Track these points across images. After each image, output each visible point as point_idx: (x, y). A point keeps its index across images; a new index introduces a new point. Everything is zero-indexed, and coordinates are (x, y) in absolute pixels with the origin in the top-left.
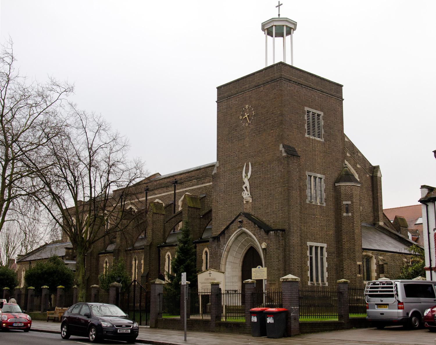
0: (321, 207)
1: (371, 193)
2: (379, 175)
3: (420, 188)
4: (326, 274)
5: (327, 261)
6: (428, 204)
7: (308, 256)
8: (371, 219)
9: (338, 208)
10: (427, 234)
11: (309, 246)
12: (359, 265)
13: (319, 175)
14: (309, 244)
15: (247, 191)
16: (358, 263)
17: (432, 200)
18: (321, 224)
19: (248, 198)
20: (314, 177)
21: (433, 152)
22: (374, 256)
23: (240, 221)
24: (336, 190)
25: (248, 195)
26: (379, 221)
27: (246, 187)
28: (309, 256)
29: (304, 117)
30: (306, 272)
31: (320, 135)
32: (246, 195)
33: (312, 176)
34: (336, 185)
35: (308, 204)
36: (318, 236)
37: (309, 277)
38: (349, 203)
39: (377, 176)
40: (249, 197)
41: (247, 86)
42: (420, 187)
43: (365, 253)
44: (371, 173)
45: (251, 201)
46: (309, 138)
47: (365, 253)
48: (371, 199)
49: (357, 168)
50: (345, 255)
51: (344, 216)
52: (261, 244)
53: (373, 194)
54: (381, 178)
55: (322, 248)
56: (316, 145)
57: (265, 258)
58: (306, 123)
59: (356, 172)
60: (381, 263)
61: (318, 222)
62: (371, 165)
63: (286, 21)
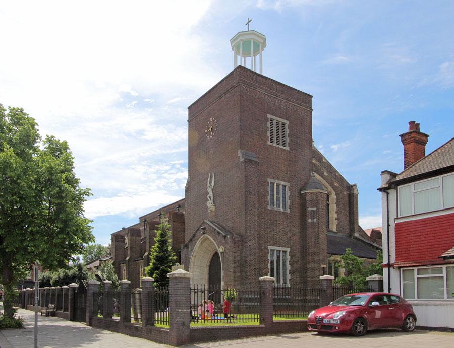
0: (284, 213)
1: (347, 208)
2: (355, 192)
3: (381, 175)
4: (289, 277)
5: (290, 264)
6: (389, 191)
8: (348, 231)
9: (303, 215)
10: (387, 227)
12: (323, 268)
16: (323, 266)
17: (393, 186)
20: (283, 185)
21: (400, 136)
23: (202, 228)
24: (302, 197)
26: (354, 233)
27: (210, 197)
29: (266, 124)
32: (210, 204)
33: (280, 184)
36: (280, 241)
38: (315, 209)
39: (353, 194)
41: (211, 99)
42: (381, 173)
43: (333, 258)
44: (348, 191)
45: (214, 210)
46: (272, 146)
47: (333, 258)
48: (348, 214)
49: (335, 186)
50: (310, 258)
52: (219, 248)
53: (350, 209)
54: (357, 195)
56: (280, 153)
57: (223, 260)
59: (334, 189)
62: (348, 184)
63: (255, 34)
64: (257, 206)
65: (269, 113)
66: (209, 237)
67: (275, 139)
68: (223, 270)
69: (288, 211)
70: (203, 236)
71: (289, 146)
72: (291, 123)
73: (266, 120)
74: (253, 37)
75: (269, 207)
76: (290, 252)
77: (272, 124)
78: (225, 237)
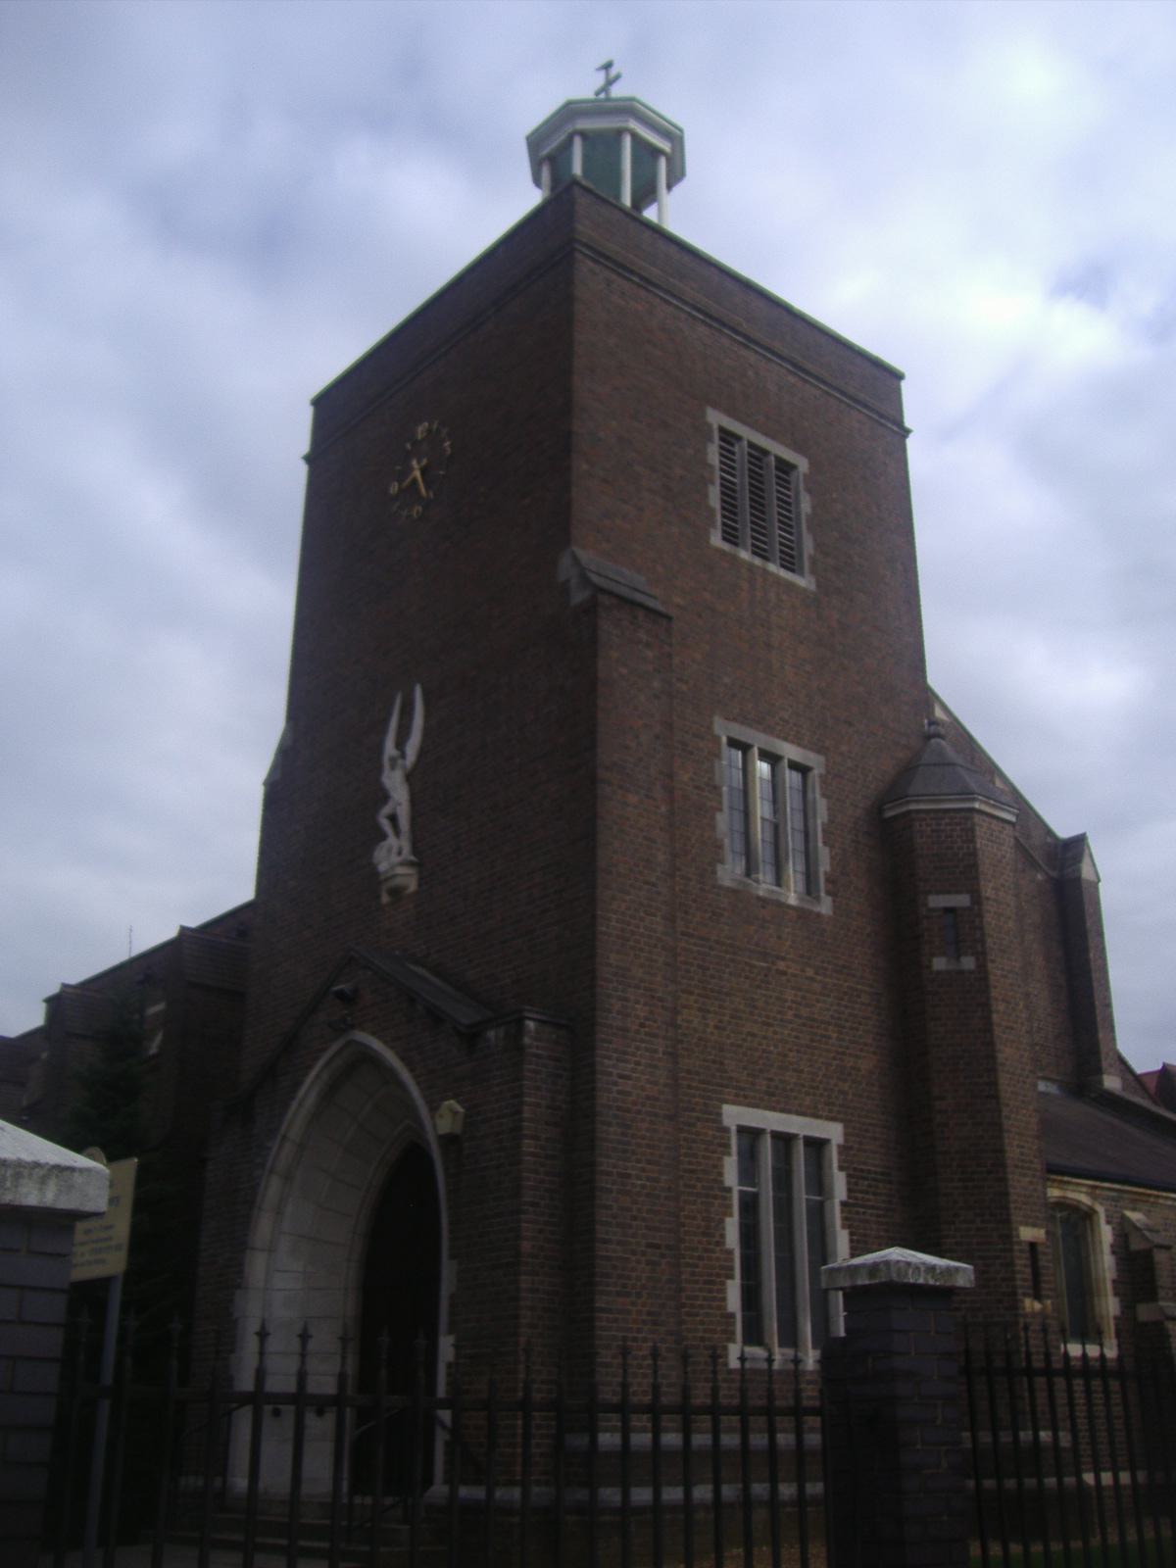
0: (803, 915)
2: (1086, 873)
7: (729, 1190)
11: (734, 1128)
12: (1033, 1245)
13: (790, 751)
14: (735, 1115)
15: (397, 832)
18: (805, 1012)
19: (400, 870)
22: (1100, 1209)
25: (400, 853)
28: (736, 1189)
30: (715, 1283)
31: (793, 523)
32: (393, 856)
34: (889, 814)
35: (728, 889)
37: (732, 1316)
38: (962, 900)
40: (402, 864)
45: (412, 886)
51: (939, 973)
52: (434, 1108)
54: (1096, 888)
55: (817, 1146)
58: (713, 483)
60: (1136, 1245)
61: (789, 994)
62: (1049, 832)
64: (661, 857)
65: (716, 406)
66: (377, 1045)
67: (772, 1325)
68: (452, 1257)
69: (825, 907)
70: (335, 1047)
71: (813, 572)
72: (814, 464)
73: (703, 431)
74: (633, 125)
75: (729, 872)
76: (844, 1149)
77: (727, 454)
78: (471, 1037)
